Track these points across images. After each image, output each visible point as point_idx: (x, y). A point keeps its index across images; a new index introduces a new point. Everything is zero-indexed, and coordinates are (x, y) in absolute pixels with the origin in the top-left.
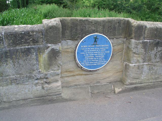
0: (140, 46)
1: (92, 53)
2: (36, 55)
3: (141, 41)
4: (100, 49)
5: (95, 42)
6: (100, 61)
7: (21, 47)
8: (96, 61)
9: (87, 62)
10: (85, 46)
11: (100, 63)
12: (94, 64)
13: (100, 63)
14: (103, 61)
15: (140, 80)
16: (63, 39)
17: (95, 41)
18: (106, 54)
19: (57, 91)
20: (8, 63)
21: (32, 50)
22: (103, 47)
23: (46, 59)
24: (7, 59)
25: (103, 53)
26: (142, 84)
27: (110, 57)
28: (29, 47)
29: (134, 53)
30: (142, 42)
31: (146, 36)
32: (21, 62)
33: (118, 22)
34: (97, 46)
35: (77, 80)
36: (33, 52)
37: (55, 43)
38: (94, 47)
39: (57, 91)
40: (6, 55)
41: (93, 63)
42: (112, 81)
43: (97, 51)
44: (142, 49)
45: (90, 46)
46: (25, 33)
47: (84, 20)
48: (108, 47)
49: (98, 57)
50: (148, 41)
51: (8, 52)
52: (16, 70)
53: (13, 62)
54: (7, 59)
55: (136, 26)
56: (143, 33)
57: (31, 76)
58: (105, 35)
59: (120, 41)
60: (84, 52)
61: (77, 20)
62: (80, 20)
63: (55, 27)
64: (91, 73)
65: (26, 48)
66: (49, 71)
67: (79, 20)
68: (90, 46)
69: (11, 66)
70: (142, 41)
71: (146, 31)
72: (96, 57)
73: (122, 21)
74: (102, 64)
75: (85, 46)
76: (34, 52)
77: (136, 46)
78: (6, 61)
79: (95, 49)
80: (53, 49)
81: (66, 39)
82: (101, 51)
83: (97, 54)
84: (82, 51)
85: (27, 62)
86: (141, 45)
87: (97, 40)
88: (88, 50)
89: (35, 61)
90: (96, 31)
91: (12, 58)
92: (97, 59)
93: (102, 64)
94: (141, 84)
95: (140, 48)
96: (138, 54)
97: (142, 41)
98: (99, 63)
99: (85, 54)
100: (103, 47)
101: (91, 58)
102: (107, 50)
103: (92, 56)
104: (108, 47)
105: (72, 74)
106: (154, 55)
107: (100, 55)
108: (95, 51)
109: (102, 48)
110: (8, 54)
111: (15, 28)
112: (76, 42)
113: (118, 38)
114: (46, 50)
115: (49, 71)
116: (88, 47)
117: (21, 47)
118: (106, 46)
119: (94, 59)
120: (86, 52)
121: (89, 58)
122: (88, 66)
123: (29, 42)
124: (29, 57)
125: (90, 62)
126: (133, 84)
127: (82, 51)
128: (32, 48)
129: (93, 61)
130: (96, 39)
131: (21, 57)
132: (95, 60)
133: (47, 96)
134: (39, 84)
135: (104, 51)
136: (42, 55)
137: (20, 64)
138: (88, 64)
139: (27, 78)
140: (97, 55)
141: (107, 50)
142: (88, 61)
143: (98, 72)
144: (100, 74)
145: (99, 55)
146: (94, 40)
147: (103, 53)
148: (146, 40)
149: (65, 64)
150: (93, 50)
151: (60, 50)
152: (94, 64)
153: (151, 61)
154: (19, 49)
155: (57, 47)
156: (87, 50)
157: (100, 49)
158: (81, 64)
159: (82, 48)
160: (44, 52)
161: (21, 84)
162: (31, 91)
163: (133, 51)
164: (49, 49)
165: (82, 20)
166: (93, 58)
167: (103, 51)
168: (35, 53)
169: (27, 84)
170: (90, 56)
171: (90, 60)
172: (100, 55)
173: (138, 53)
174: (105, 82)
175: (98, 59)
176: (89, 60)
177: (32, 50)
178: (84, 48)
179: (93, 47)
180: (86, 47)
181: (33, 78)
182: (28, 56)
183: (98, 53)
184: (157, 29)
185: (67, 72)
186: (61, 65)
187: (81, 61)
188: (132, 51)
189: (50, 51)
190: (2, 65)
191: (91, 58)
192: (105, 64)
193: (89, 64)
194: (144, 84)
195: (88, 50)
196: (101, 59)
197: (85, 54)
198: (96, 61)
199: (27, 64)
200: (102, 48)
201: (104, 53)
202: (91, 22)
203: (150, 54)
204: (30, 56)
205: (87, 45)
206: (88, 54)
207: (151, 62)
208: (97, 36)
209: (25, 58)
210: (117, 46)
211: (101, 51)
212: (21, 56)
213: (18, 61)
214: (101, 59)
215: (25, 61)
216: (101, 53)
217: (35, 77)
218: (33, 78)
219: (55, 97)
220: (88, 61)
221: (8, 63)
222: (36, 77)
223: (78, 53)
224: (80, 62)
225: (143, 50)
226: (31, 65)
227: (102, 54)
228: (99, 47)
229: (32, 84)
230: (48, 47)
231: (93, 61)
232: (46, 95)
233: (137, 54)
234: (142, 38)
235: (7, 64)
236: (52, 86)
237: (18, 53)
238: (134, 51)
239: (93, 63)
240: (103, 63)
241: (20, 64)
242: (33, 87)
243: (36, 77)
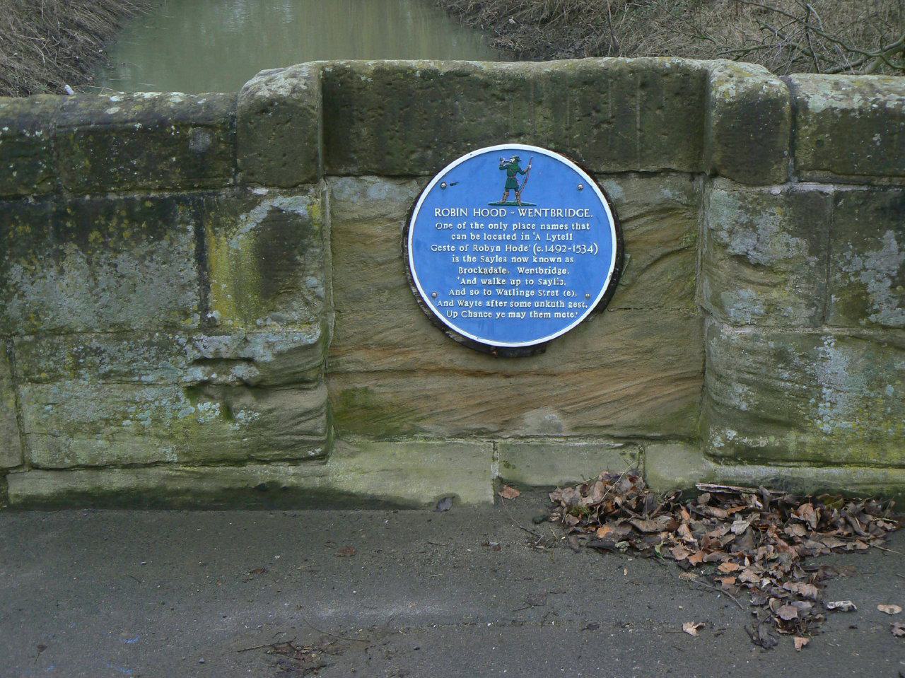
0: (772, 220)
1: (495, 253)
2: (200, 236)
3: (776, 190)
4: (538, 230)
5: (507, 189)
6: (543, 298)
7: (130, 195)
8: (522, 298)
9: (469, 297)
10: (454, 212)
11: (548, 309)
12: (512, 314)
13: (548, 309)
14: (567, 299)
15: (809, 439)
16: (342, 171)
17: (512, 185)
18: (582, 260)
19: (301, 438)
20: (65, 265)
21: (179, 209)
22: (557, 220)
23: (248, 258)
24: (61, 247)
25: (563, 254)
26: (835, 471)
27: (608, 281)
28: (167, 195)
29: (742, 259)
30: (787, 194)
31: (804, 157)
32: (125, 263)
33: (643, 85)
34: (522, 212)
35: (427, 397)
36: (182, 222)
37: (291, 188)
38: (509, 219)
39: (301, 438)
40: (57, 226)
41: (507, 309)
42: (639, 433)
43: (525, 242)
44: (793, 241)
45: (480, 212)
46: (144, 130)
47: (447, 74)
48: (585, 220)
49: (533, 275)
50: (830, 189)
51: (69, 211)
52: (103, 301)
53: (89, 262)
54: (61, 247)
55: (730, 104)
56: (783, 142)
57: (171, 343)
58: (569, 156)
59: (667, 193)
60: (452, 242)
61: (407, 73)
62: (428, 75)
63: (285, 103)
64: (504, 366)
65: (152, 200)
66: (258, 322)
67: (418, 74)
68: (480, 212)
69: (80, 280)
70: (786, 187)
71: (806, 131)
72: (521, 275)
73: (665, 79)
74: (558, 315)
75: (454, 212)
76: (188, 223)
77: (744, 219)
78: (60, 255)
79: (509, 231)
80: (280, 211)
81: (353, 169)
82: (550, 243)
83: (526, 260)
84: (443, 236)
85: (153, 266)
86: (776, 210)
87: (518, 177)
88: (476, 231)
89: (190, 265)
90: (513, 132)
91: (84, 245)
92: (529, 287)
93: (558, 315)
94: (825, 470)
95: (776, 228)
96: (770, 269)
97: (786, 187)
98: (540, 309)
99: (457, 253)
100: (557, 220)
101: (489, 276)
102: (582, 237)
103: (496, 264)
104: (585, 220)
105: (397, 361)
106: (889, 283)
107: (544, 265)
108: (511, 242)
109: (555, 226)
110: (69, 224)
111: (110, 104)
112: (411, 188)
113: (655, 174)
114: (243, 217)
115: (258, 322)
116: (469, 218)
117: (130, 195)
118: (576, 213)
119: (508, 286)
120: (461, 242)
121: (479, 276)
122: (480, 321)
123: (164, 172)
124: (165, 243)
125: (487, 298)
126: (764, 461)
127: (443, 236)
128: (180, 200)
129: (502, 298)
130: (513, 172)
131: (126, 243)
132: (516, 292)
133: (251, 459)
134: (211, 391)
135: (569, 243)
136: (226, 236)
137: (122, 276)
138: (475, 309)
139: (153, 353)
140: (522, 264)
141: (582, 237)
142: (477, 292)
143: (546, 361)
144: (557, 381)
145: (535, 265)
146: (503, 178)
147: (563, 254)
148: (810, 187)
149: (357, 300)
150: (501, 231)
151: (311, 219)
152: (512, 314)
153: (873, 318)
154: (119, 200)
155: (299, 205)
156: (467, 230)
157: (538, 230)
158: (439, 308)
159: (443, 219)
160: (235, 223)
161: (121, 382)
162: (168, 421)
163: (730, 250)
164: (260, 213)
165: (436, 72)
166: (499, 275)
167: (562, 242)
168: (190, 228)
169: (149, 384)
170: (487, 265)
171: (487, 286)
172: (544, 265)
173: (763, 259)
174: (595, 432)
175: (535, 287)
176: (480, 286)
177: (179, 209)
178: (449, 220)
179: (499, 219)
180: (461, 218)
181: (182, 353)
182: (160, 238)
183: (529, 253)
184: (882, 119)
185: (367, 347)
186: (318, 297)
187: (440, 292)
188: (726, 246)
189: (265, 221)
190: (41, 274)
191: (489, 276)
192: (578, 316)
193: (484, 308)
194: (850, 469)
195: (476, 231)
196: (552, 288)
197: (457, 253)
198: (522, 298)
199: (155, 279)
200: (555, 226)
201: (569, 253)
202: (486, 85)
203: (857, 274)
204: (171, 239)
205: (468, 205)
206: (474, 254)
207: (870, 325)
208: (517, 160)
209: (144, 247)
210: (654, 221)
211: (550, 243)
212: (126, 234)
213: (113, 261)
214: (552, 288)
215: (147, 263)
216: (549, 254)
217: (189, 347)
218: (182, 353)
219: (291, 470)
220: (477, 292)
221: (65, 265)
222: (195, 347)
223: (417, 245)
224: (432, 298)
225: (798, 245)
226: (172, 285)
227: (553, 260)
228: (536, 219)
229: (176, 387)
230: (257, 200)
231: (502, 298)
232: (243, 454)
233: (757, 266)
234: (779, 170)
235: (62, 272)
236: (273, 406)
237: (114, 222)
238: (738, 246)
239: (507, 309)
240: (565, 309)
241: (122, 276)
242: (178, 399)
243: (195, 347)
